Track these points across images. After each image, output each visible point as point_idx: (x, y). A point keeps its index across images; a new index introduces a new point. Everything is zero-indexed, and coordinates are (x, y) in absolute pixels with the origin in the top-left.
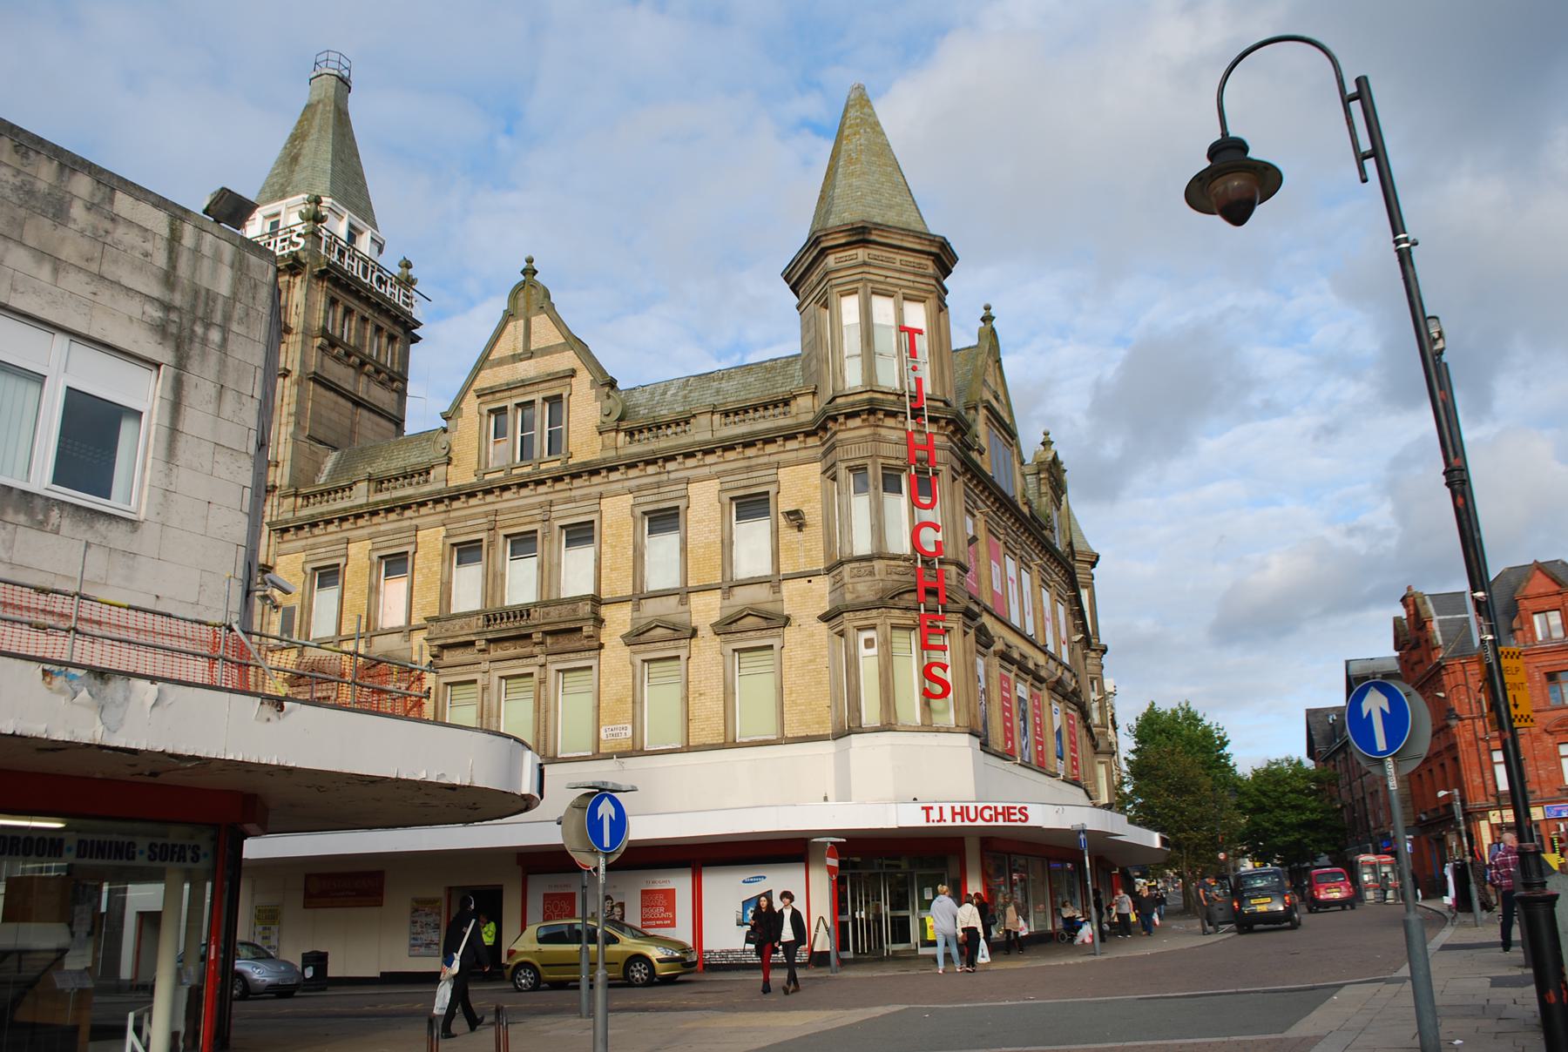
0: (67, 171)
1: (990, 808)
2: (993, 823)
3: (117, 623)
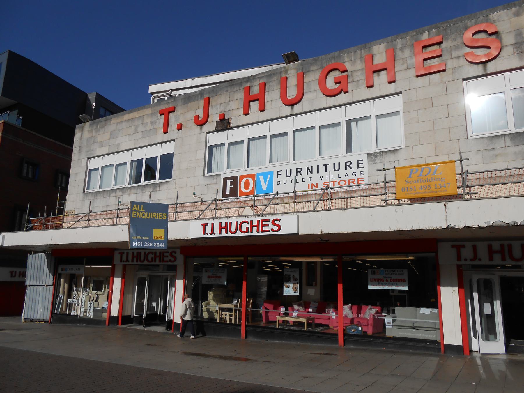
1: (248, 223)
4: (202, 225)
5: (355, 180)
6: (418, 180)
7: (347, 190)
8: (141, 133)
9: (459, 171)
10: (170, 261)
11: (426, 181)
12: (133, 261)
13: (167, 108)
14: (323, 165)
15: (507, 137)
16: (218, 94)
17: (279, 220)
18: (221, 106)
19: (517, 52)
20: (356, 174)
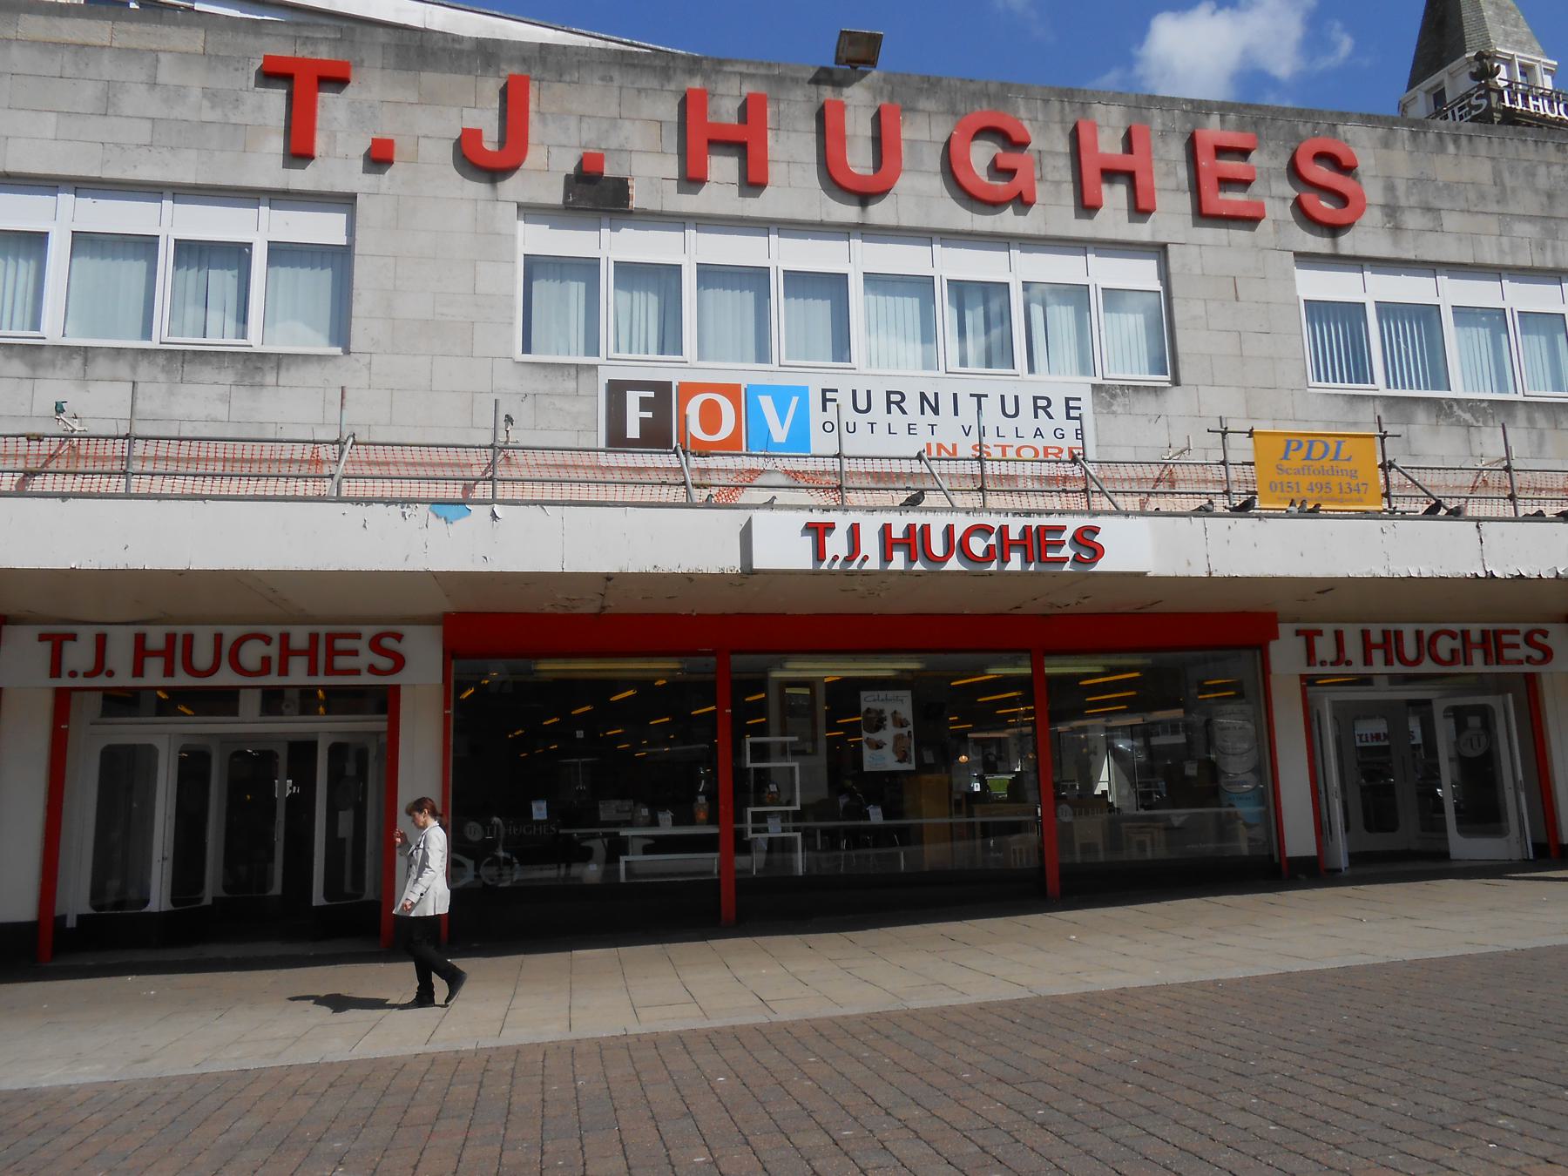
0: (1540, 144)
1: (985, 530)
3: (554, 462)
5: (1061, 451)
6: (1303, 469)
7: (884, 470)
8: (148, 125)
9: (1380, 462)
10: (1529, 659)
11: (1319, 472)
13: (299, 55)
14: (971, 395)
15: (1377, 402)
16: (567, 78)
17: (398, 637)
18: (584, 126)
19: (1388, 225)
20: (1063, 435)
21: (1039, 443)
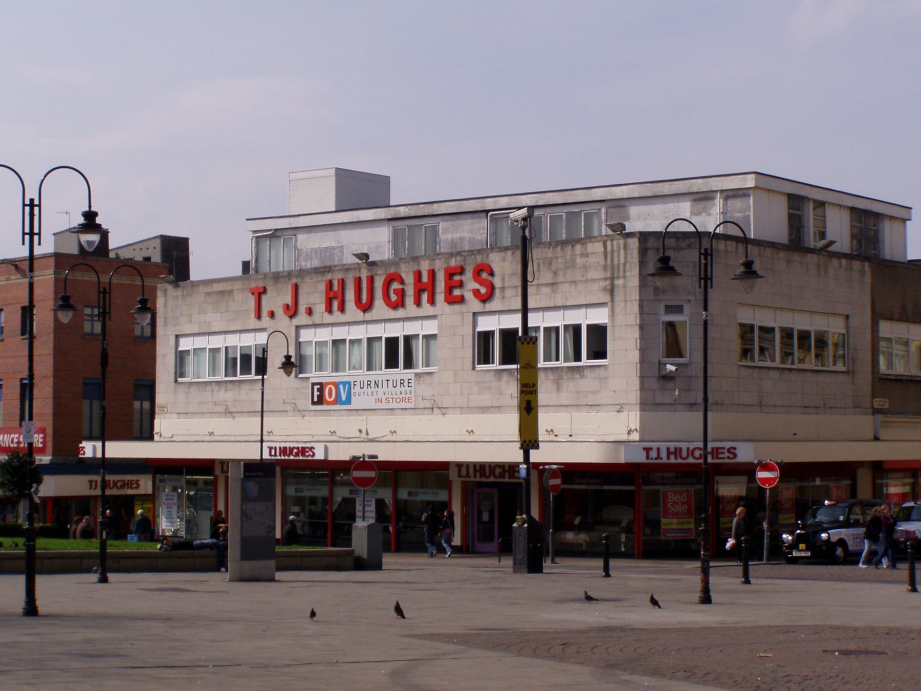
2: (501, 480)
4: (644, 449)
12: (475, 477)
21: (401, 396)
